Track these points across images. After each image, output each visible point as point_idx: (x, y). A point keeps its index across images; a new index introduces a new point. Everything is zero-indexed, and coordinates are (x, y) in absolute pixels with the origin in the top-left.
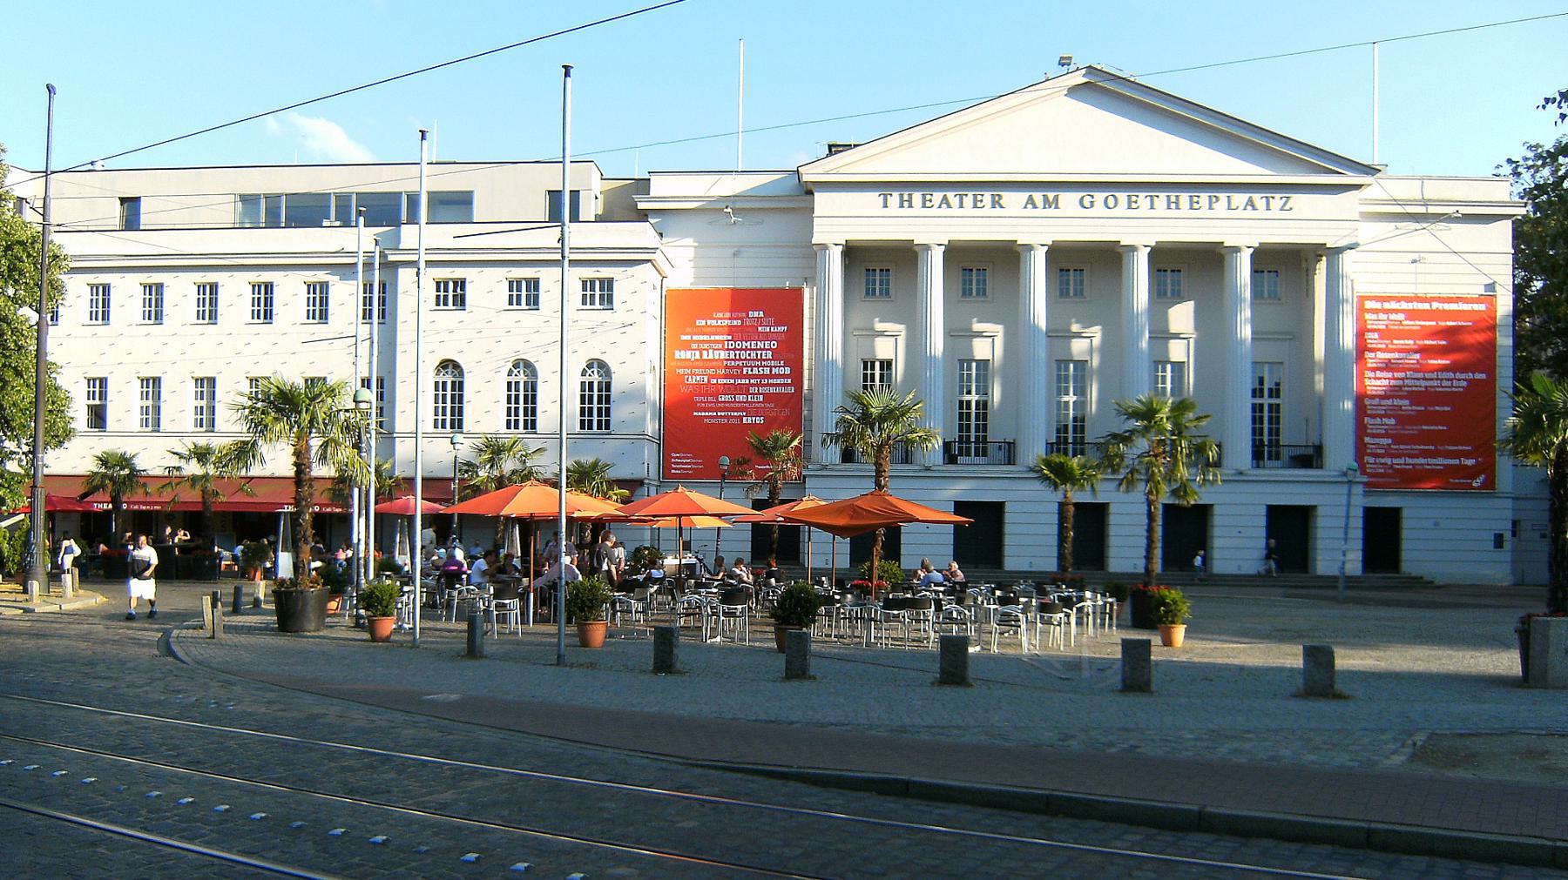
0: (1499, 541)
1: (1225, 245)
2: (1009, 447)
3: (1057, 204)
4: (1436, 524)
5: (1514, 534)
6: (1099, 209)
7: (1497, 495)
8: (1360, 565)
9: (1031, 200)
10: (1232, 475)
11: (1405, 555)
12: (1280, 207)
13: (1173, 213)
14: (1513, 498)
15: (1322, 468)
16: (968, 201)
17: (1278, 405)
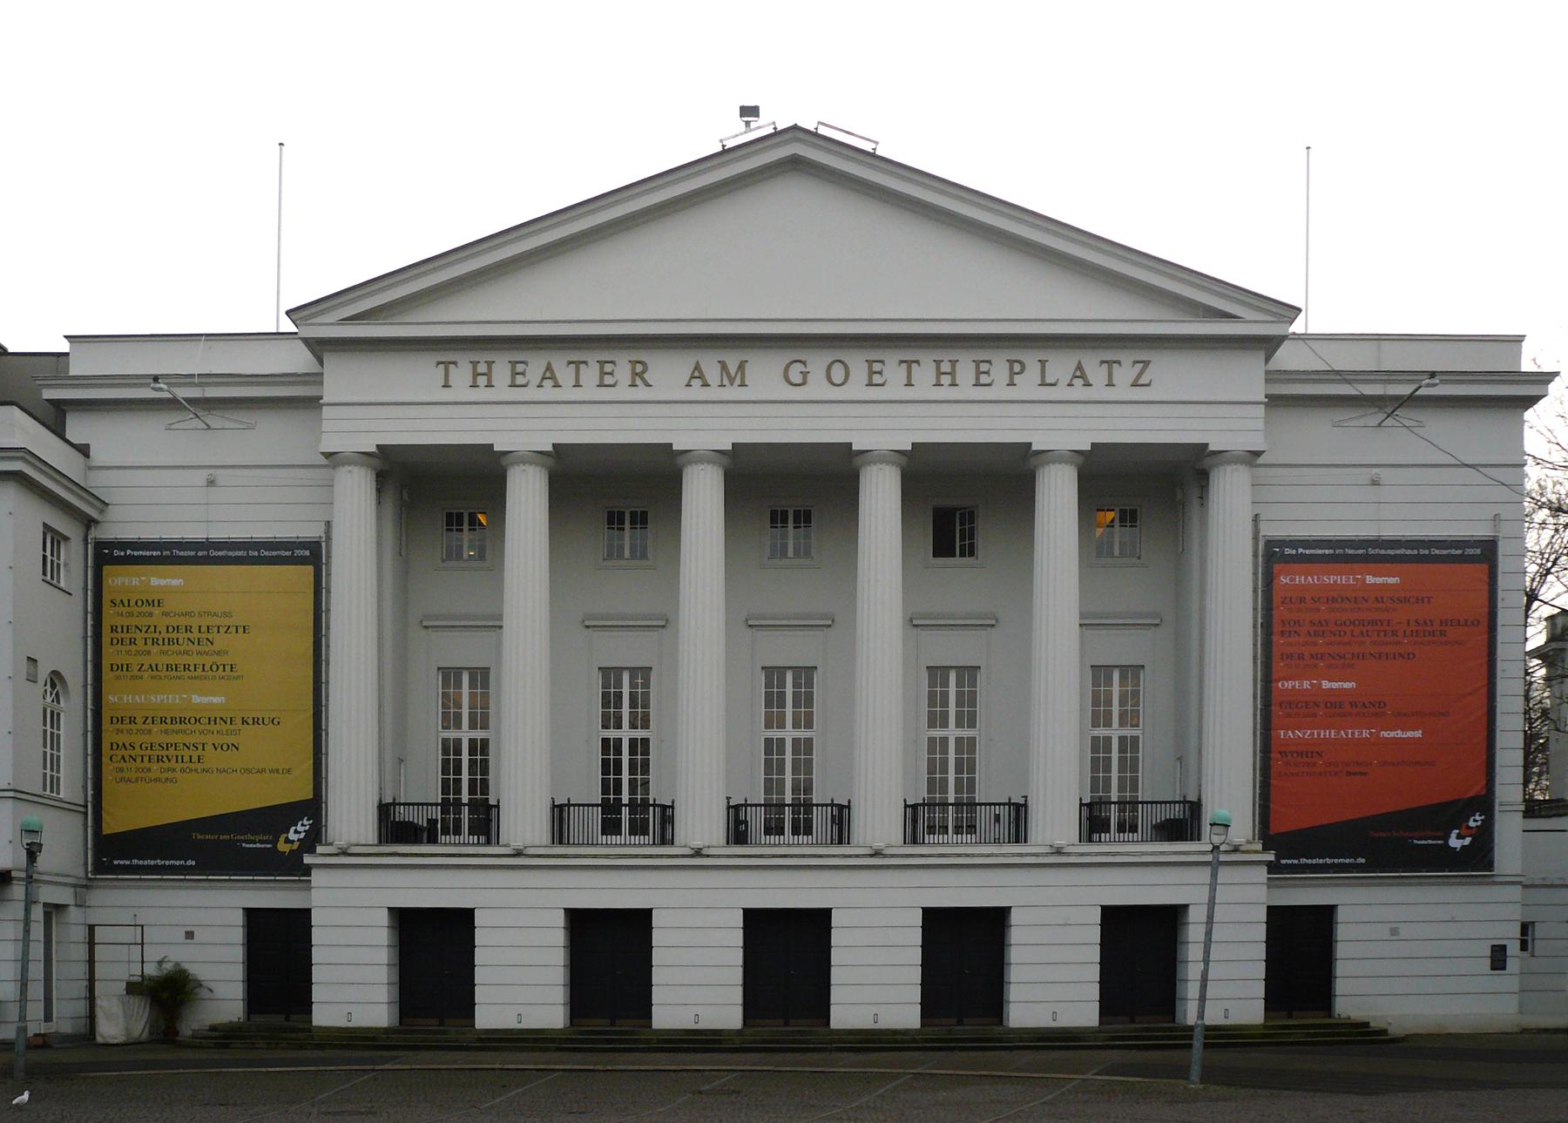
0: (1498, 958)
1: (1211, 448)
2: (841, 813)
4: (1394, 932)
6: (817, 388)
7: (1497, 879)
10: (1046, 854)
11: (1340, 986)
12: (1131, 380)
13: (945, 393)
14: (75, 886)
16: (966, 372)
17: (605, 726)
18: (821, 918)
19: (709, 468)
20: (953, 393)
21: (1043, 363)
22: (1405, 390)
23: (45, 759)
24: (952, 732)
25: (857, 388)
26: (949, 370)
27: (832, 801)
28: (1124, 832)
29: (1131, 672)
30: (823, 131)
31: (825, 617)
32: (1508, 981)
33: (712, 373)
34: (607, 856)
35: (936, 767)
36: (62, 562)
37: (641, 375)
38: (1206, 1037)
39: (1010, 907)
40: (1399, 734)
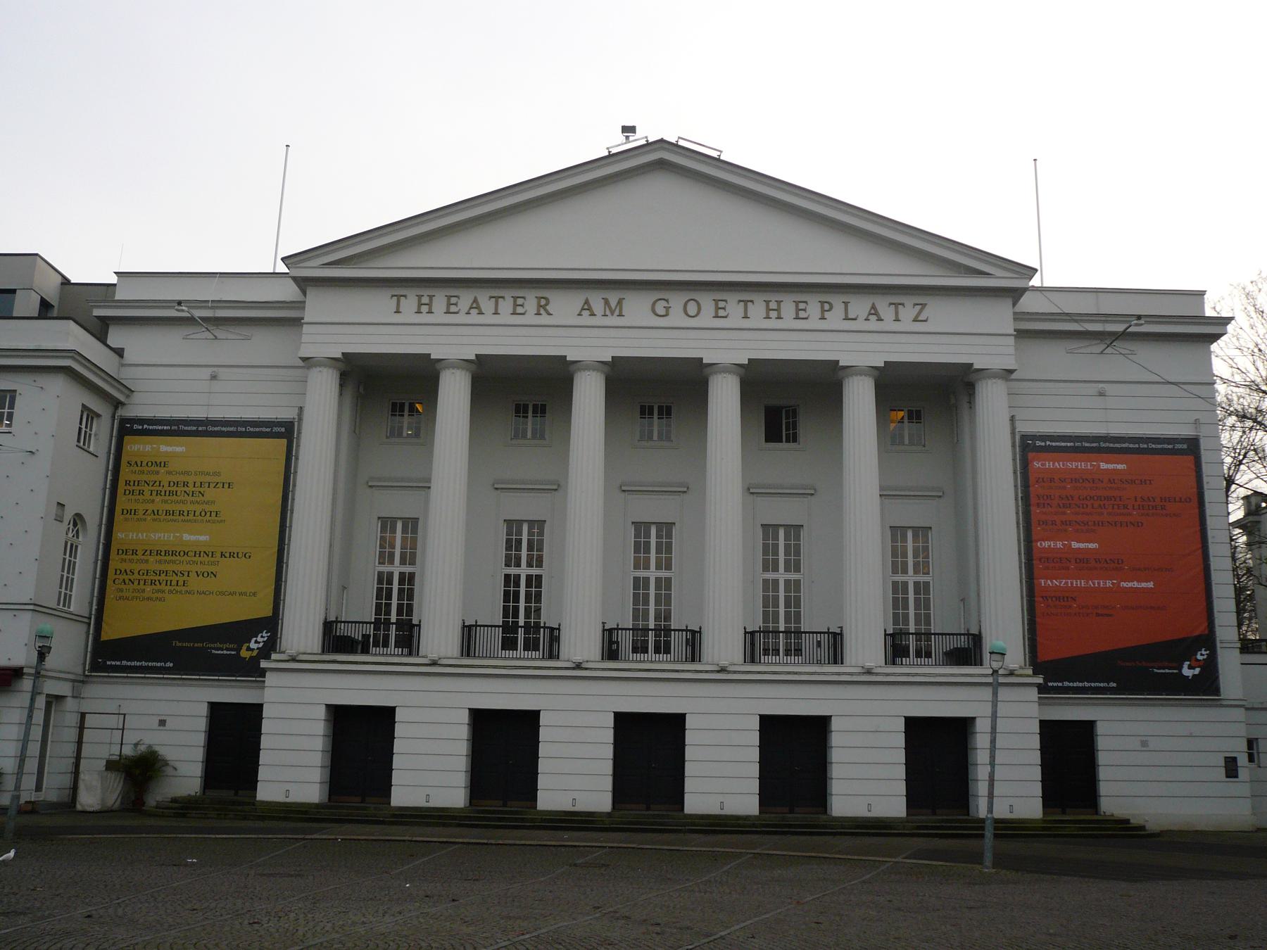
0: (1231, 768)
3: (621, 310)
4: (1144, 744)
5: (1251, 759)
6: (677, 318)
8: (903, 801)
9: (587, 307)
11: (1104, 789)
12: (913, 317)
16: (788, 308)
21: (846, 304)
22: (1119, 328)
23: (62, 581)
24: (782, 576)
25: (706, 319)
26: (775, 307)
27: (476, 622)
28: (660, 653)
30: (681, 143)
33: (598, 306)
34: (504, 667)
35: (898, 602)
36: (93, 432)
37: (544, 307)
39: (831, 716)
40: (1135, 584)
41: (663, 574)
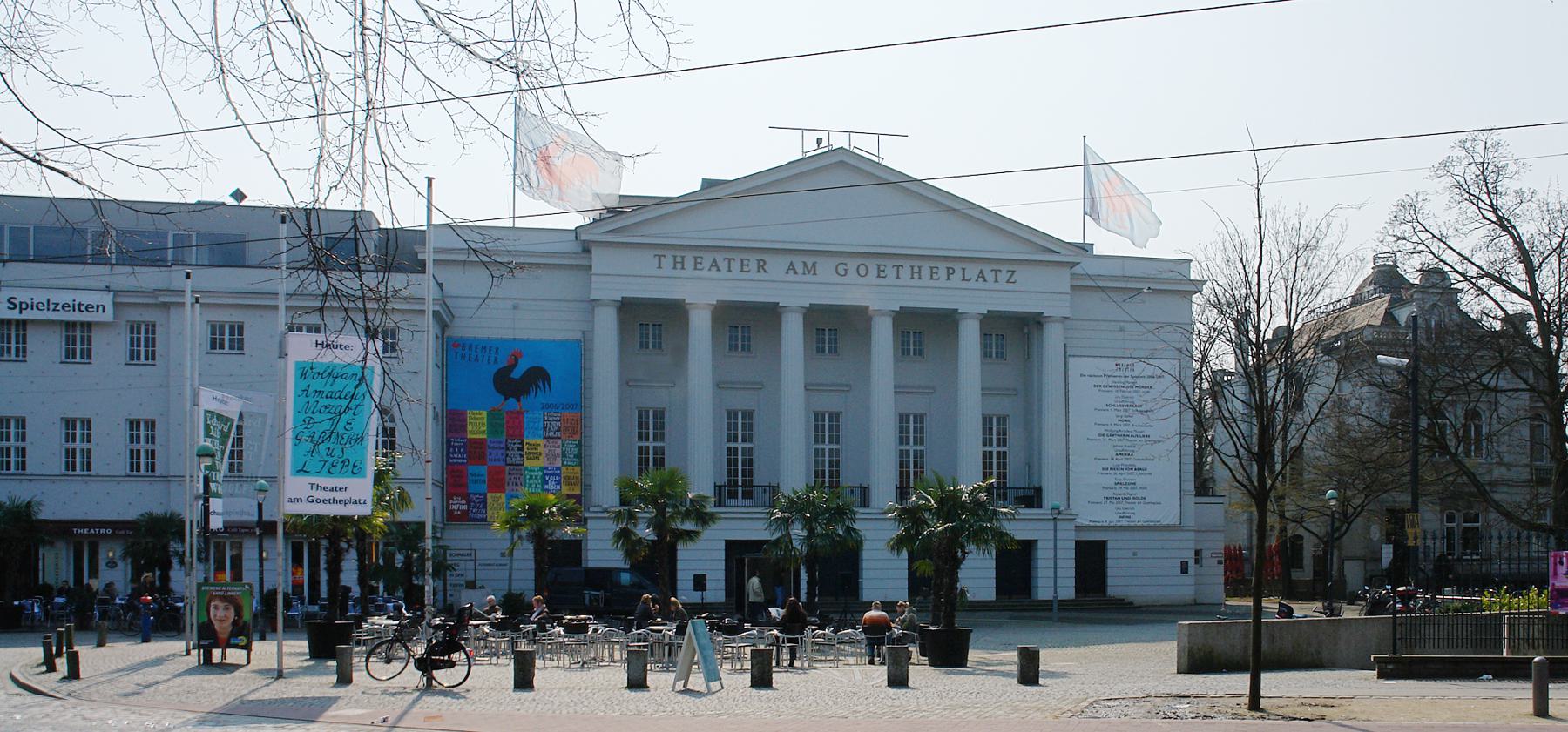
0: (1184, 569)
3: (815, 271)
4: (1135, 554)
5: (1197, 561)
9: (792, 266)
11: (1110, 581)
13: (915, 282)
14: (1195, 531)
15: (868, 507)
16: (1003, 276)
18: (1105, 542)
19: (797, 315)
20: (920, 283)
21: (964, 269)
24: (827, 447)
29: (1002, 420)
31: (847, 386)
32: (1188, 579)
35: (731, 462)
38: (1059, 605)
41: (834, 447)
